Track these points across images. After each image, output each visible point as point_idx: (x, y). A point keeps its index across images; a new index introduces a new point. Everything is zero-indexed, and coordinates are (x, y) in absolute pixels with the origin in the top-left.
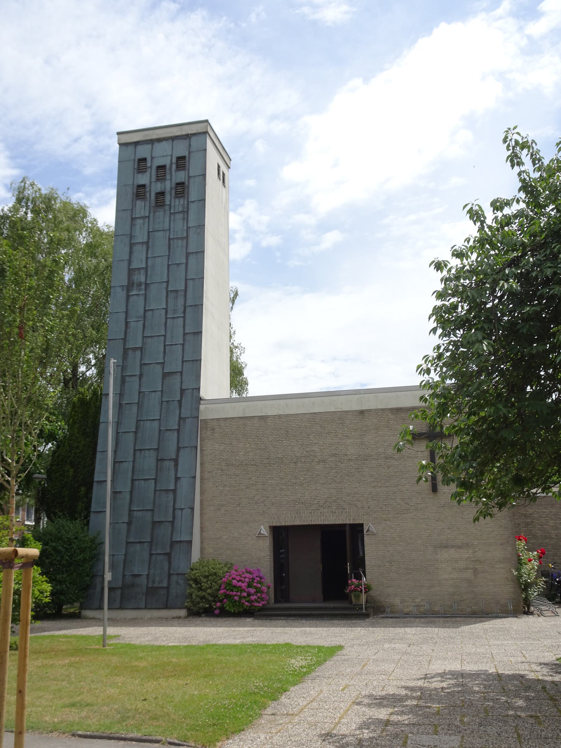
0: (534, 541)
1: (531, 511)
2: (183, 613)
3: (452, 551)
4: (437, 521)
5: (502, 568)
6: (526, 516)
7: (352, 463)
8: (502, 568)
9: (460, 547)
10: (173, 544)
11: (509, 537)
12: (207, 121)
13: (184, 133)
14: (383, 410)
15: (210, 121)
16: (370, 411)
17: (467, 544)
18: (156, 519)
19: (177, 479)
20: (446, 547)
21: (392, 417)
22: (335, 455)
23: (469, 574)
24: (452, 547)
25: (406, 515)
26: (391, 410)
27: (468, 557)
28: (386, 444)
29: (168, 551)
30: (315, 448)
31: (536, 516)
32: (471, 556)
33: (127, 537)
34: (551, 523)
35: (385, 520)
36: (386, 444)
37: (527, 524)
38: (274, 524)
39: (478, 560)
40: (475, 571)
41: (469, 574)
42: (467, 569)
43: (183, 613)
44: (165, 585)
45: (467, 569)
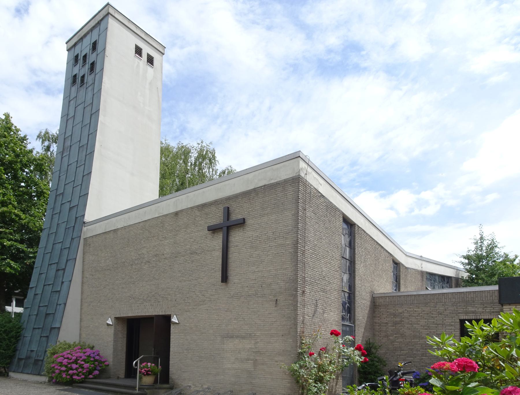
0: (401, 340)
1: (400, 310)
2: (45, 379)
3: (237, 341)
4: (226, 311)
5: (281, 361)
6: (395, 315)
7: (166, 261)
8: (281, 361)
9: (243, 338)
10: (52, 329)
11: (291, 328)
12: (108, 4)
13: (97, 22)
14: (192, 208)
15: (111, 3)
16: (182, 211)
17: (250, 334)
18: (48, 312)
19: (63, 282)
20: (232, 337)
21: (198, 213)
22: (156, 255)
23: (249, 366)
24: (237, 337)
25: (202, 307)
26: (198, 206)
27: (251, 348)
28: (192, 240)
29: (48, 335)
30: (144, 251)
31: (406, 315)
32: (253, 346)
33: (34, 325)
34: (423, 322)
35: (186, 311)
36: (192, 240)
37: (395, 323)
38: (117, 316)
39: (259, 352)
40: (255, 361)
41: (249, 366)
42: (248, 359)
43: (45, 379)
44: (42, 359)
45: (248, 359)
